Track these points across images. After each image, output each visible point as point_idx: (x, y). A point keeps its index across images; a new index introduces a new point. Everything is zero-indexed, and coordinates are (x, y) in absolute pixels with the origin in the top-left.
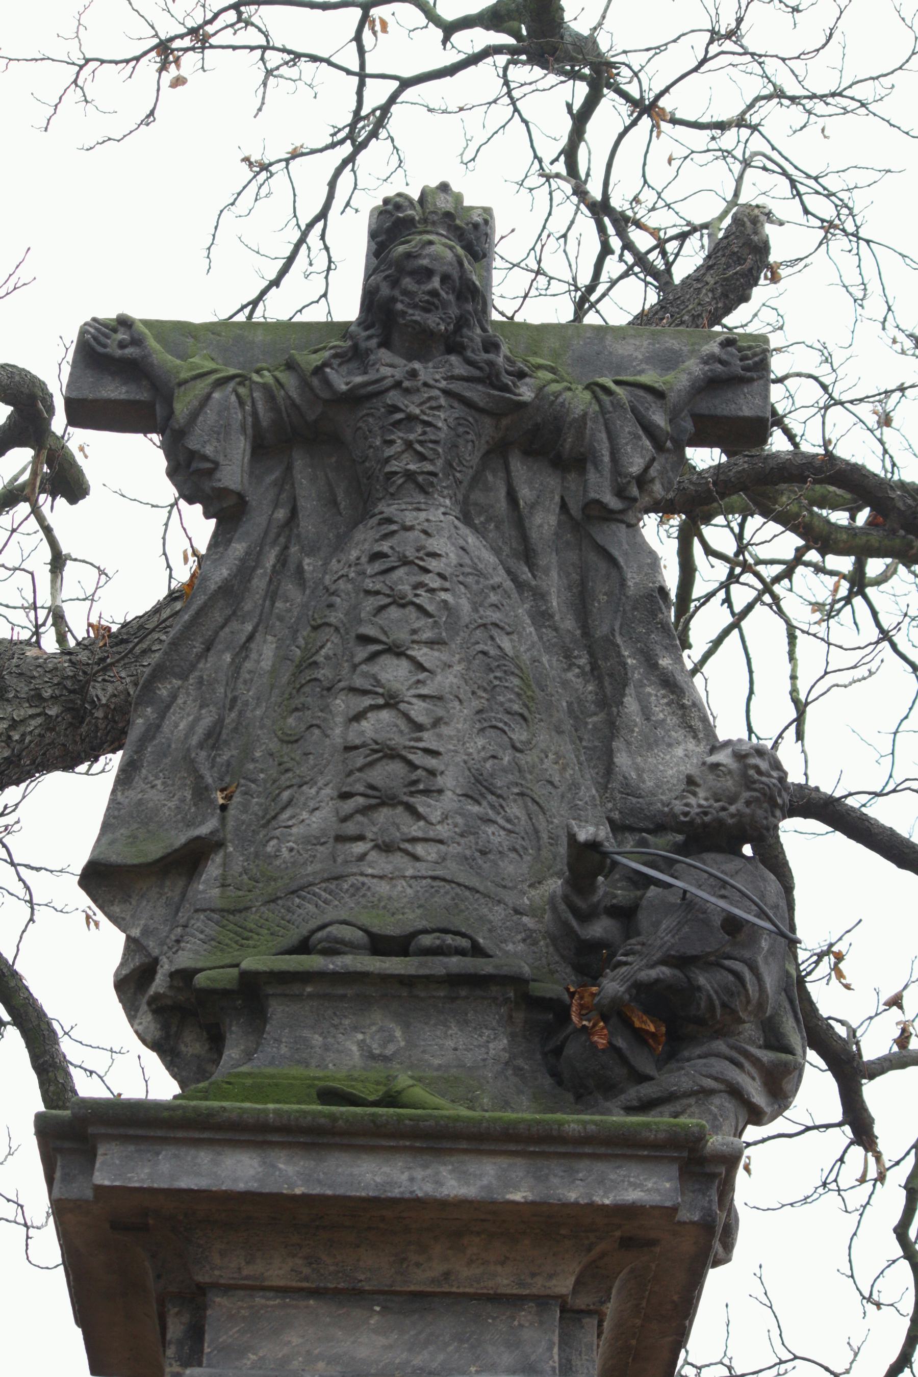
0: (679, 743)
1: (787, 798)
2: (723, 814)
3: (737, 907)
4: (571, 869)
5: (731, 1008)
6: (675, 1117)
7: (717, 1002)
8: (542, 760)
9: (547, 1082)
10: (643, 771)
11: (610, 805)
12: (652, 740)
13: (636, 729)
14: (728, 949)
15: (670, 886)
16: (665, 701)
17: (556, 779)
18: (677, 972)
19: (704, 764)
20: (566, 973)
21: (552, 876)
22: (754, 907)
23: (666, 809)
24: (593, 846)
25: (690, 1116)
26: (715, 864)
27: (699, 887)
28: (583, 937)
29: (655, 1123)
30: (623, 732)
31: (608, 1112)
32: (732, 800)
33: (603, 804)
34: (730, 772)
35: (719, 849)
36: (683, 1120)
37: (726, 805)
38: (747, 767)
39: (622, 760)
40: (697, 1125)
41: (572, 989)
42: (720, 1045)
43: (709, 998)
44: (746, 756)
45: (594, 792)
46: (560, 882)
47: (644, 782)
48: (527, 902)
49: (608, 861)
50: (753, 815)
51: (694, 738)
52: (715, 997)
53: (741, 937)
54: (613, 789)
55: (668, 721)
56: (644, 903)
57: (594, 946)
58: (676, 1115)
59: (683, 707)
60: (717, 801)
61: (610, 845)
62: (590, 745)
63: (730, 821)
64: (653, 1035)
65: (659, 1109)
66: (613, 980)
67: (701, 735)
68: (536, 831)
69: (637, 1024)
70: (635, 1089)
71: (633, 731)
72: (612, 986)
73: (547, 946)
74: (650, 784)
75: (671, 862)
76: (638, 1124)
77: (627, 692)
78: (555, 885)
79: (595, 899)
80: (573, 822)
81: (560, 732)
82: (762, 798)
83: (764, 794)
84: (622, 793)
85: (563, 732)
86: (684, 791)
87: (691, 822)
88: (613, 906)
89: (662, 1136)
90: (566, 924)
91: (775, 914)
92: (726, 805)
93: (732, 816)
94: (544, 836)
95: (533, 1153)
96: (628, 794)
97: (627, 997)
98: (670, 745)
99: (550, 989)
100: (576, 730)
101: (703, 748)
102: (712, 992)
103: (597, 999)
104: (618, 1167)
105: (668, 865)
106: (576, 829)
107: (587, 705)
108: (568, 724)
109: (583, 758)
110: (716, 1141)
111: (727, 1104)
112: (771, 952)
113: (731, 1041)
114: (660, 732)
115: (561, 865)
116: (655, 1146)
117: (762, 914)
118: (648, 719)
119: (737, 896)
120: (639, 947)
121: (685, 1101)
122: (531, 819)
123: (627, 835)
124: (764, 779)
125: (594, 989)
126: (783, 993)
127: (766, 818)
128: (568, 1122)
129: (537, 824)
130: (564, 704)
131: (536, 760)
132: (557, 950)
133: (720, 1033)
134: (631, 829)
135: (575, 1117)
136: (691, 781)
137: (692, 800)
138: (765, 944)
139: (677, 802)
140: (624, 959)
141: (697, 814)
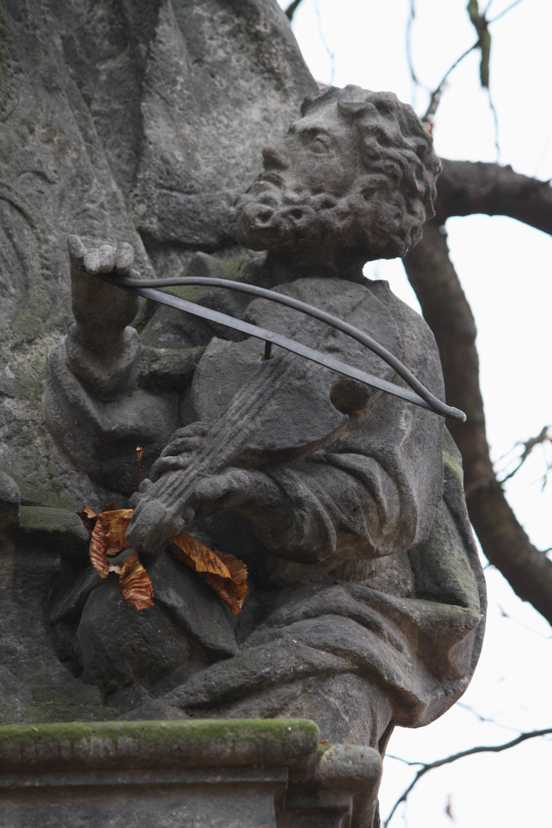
0: (252, 99)
1: (431, 179)
2: (326, 213)
3: (357, 366)
4: (79, 317)
5: (354, 533)
6: (272, 716)
7: (330, 524)
8: (23, 138)
9: (56, 670)
10: (195, 148)
11: (142, 208)
12: (207, 95)
13: (180, 79)
14: (344, 436)
15: (245, 336)
16: (227, 28)
17: (50, 168)
18: (261, 477)
19: (292, 130)
20: (80, 488)
21: (50, 330)
22: (384, 365)
23: (232, 209)
24: (114, 276)
25: (294, 715)
26: (317, 296)
27: (292, 335)
28: (106, 428)
29: (232, 729)
30: (157, 85)
31: (160, 714)
32: (341, 189)
33: (130, 207)
34: (335, 142)
35: (323, 272)
36: (283, 720)
37: (331, 198)
38: (362, 132)
39: (159, 132)
40: (302, 727)
41: (91, 515)
42: (339, 595)
43: (317, 516)
44: (361, 114)
45: (114, 186)
46: (63, 339)
47: (197, 167)
48: (12, 376)
49: (142, 301)
50: (376, 213)
51: (277, 88)
52: (326, 515)
53: (367, 415)
54: (146, 181)
55: (234, 62)
56: (202, 366)
57: (122, 443)
58: (273, 713)
59: (257, 37)
60: (316, 191)
61: (144, 272)
62: (104, 109)
63: (339, 224)
64: (228, 583)
65: (242, 706)
66: (155, 496)
67: (289, 84)
68: (21, 257)
69: (201, 567)
70: (202, 673)
71: (174, 82)
72: (155, 505)
73: (47, 446)
74: (206, 170)
75: (246, 297)
76: (204, 731)
77: (162, 15)
78: (55, 344)
79: (123, 364)
80: (79, 239)
81: (51, 89)
82: (391, 184)
83: (394, 177)
84: (162, 187)
85: (57, 89)
86: (260, 177)
87: (275, 229)
88: (153, 374)
89: (243, 748)
90: (75, 408)
91: (420, 375)
92: (331, 198)
93: (343, 215)
94: (35, 263)
95: (32, 789)
96: (171, 189)
97: (180, 522)
98: (238, 103)
99: (53, 516)
100: (80, 85)
101: (292, 105)
102: (321, 508)
103: (131, 528)
104: (174, 806)
105: (239, 304)
106: (83, 250)
107: (97, 41)
108: (65, 77)
109: (93, 132)
110: (335, 755)
111: (354, 692)
112: (417, 438)
113: (358, 587)
114: (220, 82)
115: (64, 311)
116: (233, 766)
117: (399, 376)
118: (199, 61)
119: (356, 348)
120: (196, 439)
121: (285, 691)
122: (10, 236)
123: (173, 256)
124: (392, 151)
125: (126, 513)
126: (442, 505)
127: (399, 216)
128: (87, 734)
129: (20, 244)
130: (58, 41)
131: (15, 137)
132: (64, 451)
133: (341, 575)
134: (180, 246)
135: (99, 725)
136: (270, 161)
137: (275, 193)
138: (405, 425)
139: (250, 197)
140: (172, 459)
141: (284, 215)
